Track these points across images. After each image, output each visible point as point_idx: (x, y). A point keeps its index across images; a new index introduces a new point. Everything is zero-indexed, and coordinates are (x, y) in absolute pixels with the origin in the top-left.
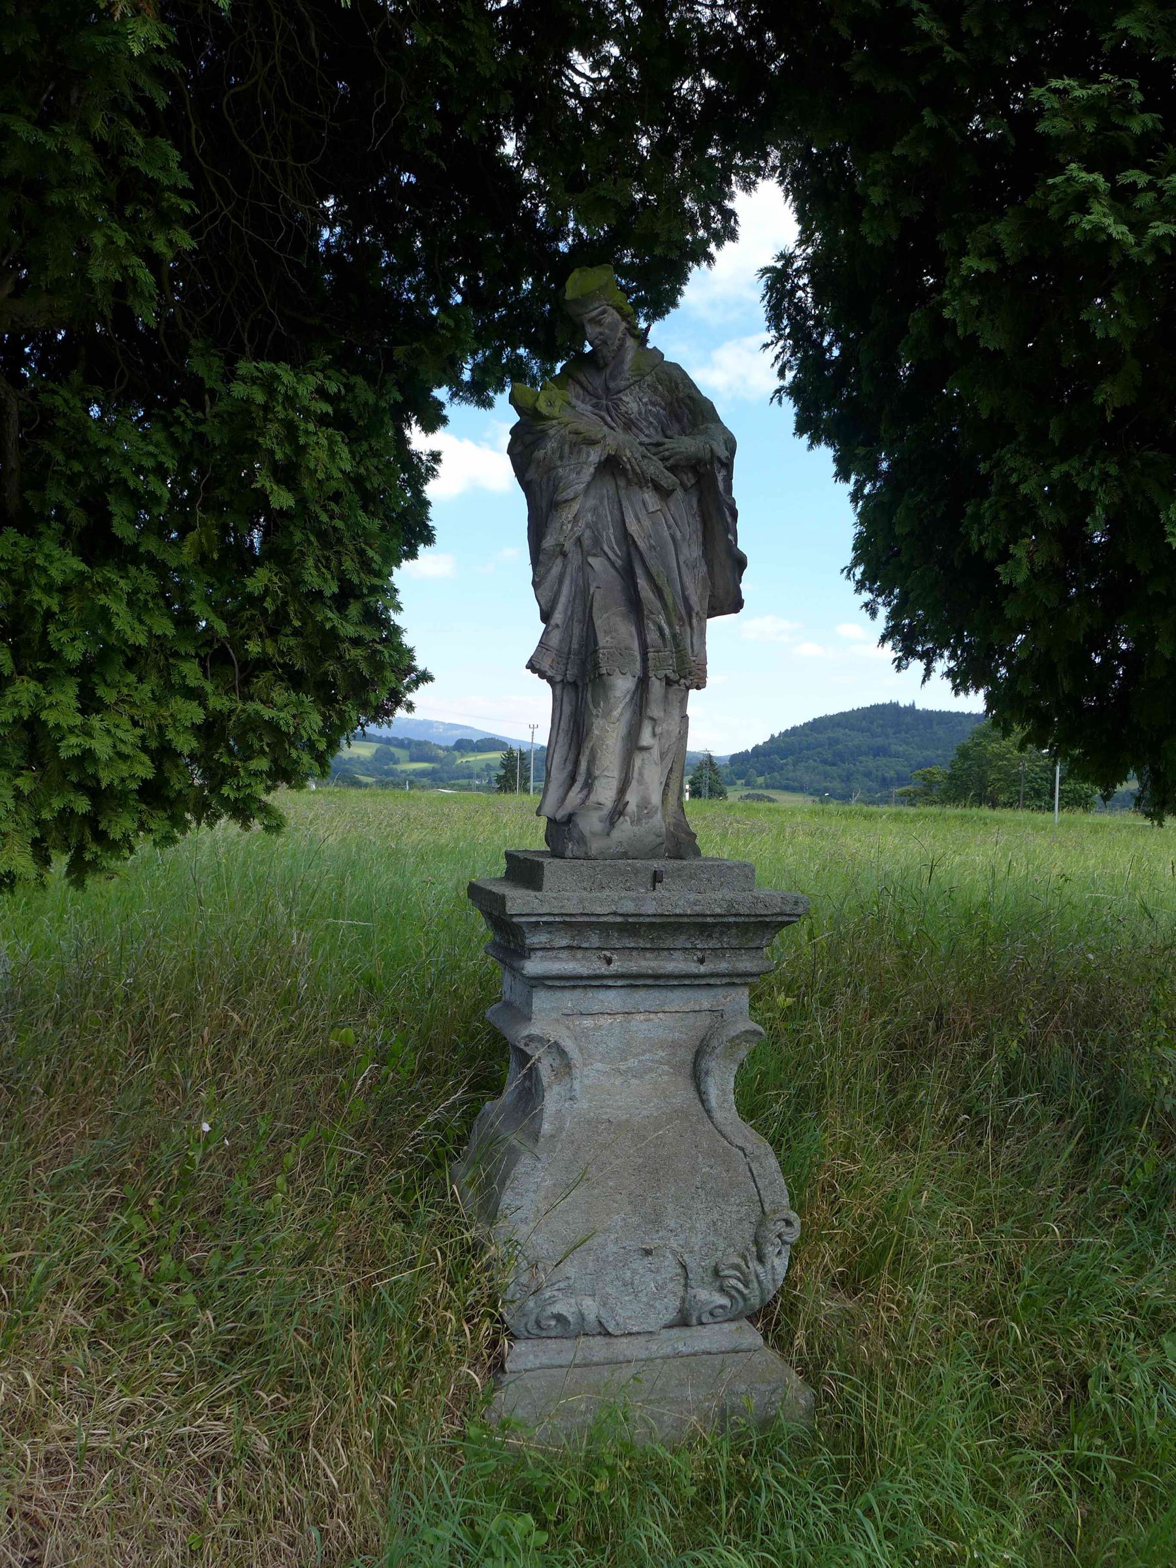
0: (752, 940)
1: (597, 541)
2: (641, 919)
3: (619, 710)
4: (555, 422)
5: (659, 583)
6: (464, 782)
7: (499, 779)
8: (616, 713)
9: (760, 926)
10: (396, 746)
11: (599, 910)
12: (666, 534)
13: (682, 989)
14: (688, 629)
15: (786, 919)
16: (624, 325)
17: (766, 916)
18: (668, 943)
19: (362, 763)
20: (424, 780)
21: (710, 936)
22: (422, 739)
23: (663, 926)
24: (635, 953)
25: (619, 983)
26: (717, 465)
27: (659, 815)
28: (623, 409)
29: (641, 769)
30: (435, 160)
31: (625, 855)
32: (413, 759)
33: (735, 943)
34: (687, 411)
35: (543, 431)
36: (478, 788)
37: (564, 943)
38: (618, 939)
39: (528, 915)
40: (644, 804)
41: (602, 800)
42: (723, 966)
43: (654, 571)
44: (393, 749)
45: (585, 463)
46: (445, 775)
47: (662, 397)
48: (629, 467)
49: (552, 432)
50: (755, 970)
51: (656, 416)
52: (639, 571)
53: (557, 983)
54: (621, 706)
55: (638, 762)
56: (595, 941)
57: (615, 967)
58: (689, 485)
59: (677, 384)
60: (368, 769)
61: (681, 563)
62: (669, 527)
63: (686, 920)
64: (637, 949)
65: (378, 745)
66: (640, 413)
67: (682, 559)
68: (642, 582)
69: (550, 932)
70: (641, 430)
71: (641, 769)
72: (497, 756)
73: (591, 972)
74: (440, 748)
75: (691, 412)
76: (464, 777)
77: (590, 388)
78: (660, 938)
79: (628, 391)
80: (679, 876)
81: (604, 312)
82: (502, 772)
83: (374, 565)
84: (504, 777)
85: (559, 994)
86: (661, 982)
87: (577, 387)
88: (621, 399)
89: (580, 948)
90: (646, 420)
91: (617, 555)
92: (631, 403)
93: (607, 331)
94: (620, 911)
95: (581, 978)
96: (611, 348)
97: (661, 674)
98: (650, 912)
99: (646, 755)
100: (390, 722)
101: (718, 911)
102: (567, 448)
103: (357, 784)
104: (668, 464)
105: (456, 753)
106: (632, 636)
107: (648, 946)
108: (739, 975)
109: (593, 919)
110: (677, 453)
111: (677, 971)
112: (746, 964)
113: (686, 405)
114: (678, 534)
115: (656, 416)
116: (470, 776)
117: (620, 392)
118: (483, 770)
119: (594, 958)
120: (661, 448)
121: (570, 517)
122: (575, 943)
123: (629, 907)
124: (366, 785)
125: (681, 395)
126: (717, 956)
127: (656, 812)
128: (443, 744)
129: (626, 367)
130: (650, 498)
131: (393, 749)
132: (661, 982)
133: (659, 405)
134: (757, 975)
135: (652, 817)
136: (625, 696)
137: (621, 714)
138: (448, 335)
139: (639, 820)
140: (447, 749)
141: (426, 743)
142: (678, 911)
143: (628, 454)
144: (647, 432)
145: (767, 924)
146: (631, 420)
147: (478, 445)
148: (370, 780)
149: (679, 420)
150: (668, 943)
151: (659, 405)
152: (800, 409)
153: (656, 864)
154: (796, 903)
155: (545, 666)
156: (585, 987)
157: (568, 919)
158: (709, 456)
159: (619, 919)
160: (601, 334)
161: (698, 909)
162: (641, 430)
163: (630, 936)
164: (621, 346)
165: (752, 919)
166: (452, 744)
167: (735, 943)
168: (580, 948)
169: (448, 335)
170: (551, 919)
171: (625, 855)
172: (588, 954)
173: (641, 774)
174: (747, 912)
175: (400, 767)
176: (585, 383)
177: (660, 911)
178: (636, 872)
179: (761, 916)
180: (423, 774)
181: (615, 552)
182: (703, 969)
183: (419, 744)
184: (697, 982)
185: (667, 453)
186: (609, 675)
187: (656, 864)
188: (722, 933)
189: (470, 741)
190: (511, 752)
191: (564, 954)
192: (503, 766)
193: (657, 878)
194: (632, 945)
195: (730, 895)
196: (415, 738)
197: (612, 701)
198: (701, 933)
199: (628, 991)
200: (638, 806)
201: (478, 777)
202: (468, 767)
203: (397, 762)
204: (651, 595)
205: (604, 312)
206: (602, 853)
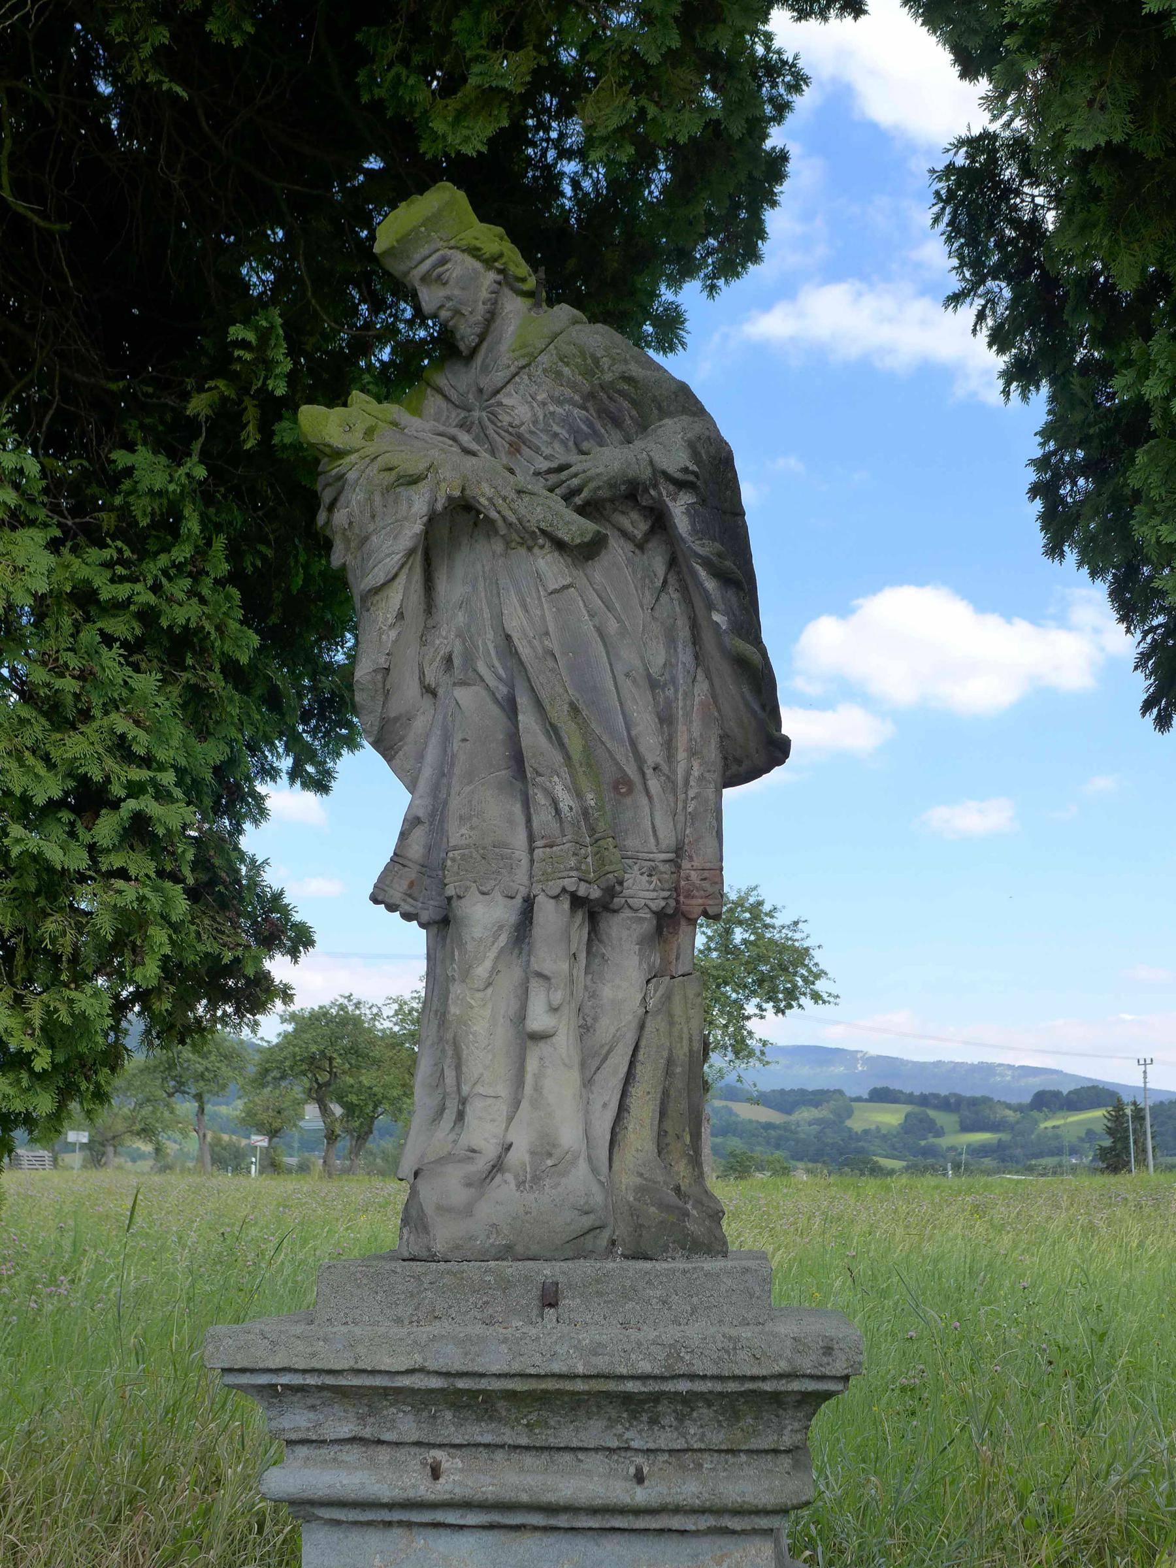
0: (755, 1433)
1: (469, 659)
2: (483, 1384)
3: (488, 964)
4: (353, 458)
5: (553, 715)
6: (1050, 1161)
7: (1103, 1154)
8: (482, 971)
9: (771, 1405)
10: (936, 1107)
11: (386, 1362)
12: (588, 627)
13: (617, 1538)
14: (644, 801)
15: (812, 1386)
16: (492, 276)
17: (764, 1378)
18: (567, 1436)
19: (885, 1138)
20: (986, 1160)
21: (654, 1421)
22: (978, 1095)
23: (543, 1399)
24: (500, 1455)
25: (472, 1519)
26: (665, 489)
27: (582, 1167)
28: (506, 419)
29: (538, 1077)
30: (165, 87)
31: (506, 1252)
32: (965, 1128)
33: (717, 1438)
34: (626, 404)
35: (340, 477)
36: (1073, 1170)
37: (346, 1430)
38: (458, 1426)
39: (243, 1371)
40: (545, 1147)
41: (477, 1143)
42: (690, 1490)
43: (544, 695)
44: (932, 1113)
45: (406, 518)
46: (1019, 1152)
47: (573, 386)
48: (494, 515)
49: (352, 476)
50: (767, 1500)
51: (565, 421)
52: (523, 701)
53: (451, 1518)
54: (492, 955)
55: (532, 1065)
56: (407, 1426)
57: (444, 1488)
58: (639, 535)
59: (596, 361)
60: (893, 1148)
61: (621, 677)
62: (592, 615)
63: (580, 1386)
64: (502, 1446)
65: (908, 1108)
66: (535, 422)
67: (619, 668)
68: (527, 719)
69: (313, 1408)
70: (537, 450)
71: (538, 1077)
72: (1097, 1116)
73: (397, 1494)
74: (1009, 1106)
75: (634, 403)
76: (1051, 1154)
77: (454, 396)
78: (547, 1425)
79: (510, 387)
80: (599, 1294)
81: (443, 261)
82: (1107, 1142)
83: (135, 748)
84: (1112, 1149)
85: (355, 1538)
86: (618, 1522)
87: (439, 398)
88: (500, 404)
89: (380, 1442)
90: (546, 431)
91: (500, 679)
92: (518, 407)
93: (457, 292)
94: (431, 1365)
95: (622, 1511)
96: (472, 319)
97: (555, 887)
98: (495, 1369)
99: (544, 1048)
100: (256, 1023)
101: (645, 1367)
102: (377, 498)
103: (876, 1171)
104: (578, 500)
105: (1035, 1113)
106: (511, 822)
107: (524, 1441)
108: (737, 1512)
109: (378, 1381)
110: (591, 479)
111: (583, 1499)
112: (747, 1484)
113: (621, 393)
114: (612, 626)
115: (565, 421)
116: (1058, 1152)
117: (498, 392)
118: (1081, 1140)
119: (414, 1464)
120: (564, 475)
121: (391, 617)
122: (367, 1433)
123: (451, 1358)
124: (891, 1172)
125: (608, 377)
126: (683, 1467)
127: (574, 1162)
128: (1014, 1101)
129: (503, 348)
130: (549, 566)
131: (932, 1113)
132: (562, 1521)
133: (571, 401)
134: (783, 1511)
135: (564, 1174)
136: (496, 938)
137: (495, 971)
138: (248, 356)
139: (536, 1179)
140: (1019, 1108)
141: (986, 1100)
142: (557, 1367)
143: (488, 490)
144: (547, 451)
145: (776, 1399)
146: (519, 436)
147: (1039, 626)
148: (898, 1164)
149: (617, 423)
150: (567, 1436)
151: (571, 401)
152: (1054, 392)
153: (548, 1270)
154: (828, 1350)
155: (396, 896)
156: (409, 1525)
157: (330, 1380)
158: (648, 472)
159: (436, 1383)
160: (449, 298)
161: (601, 1364)
162: (537, 450)
163: (479, 1420)
164: (491, 316)
165: (732, 1387)
166: (1027, 1099)
167: (717, 1438)
168: (380, 1442)
169: (248, 356)
170: (297, 1380)
171: (506, 1252)
172: (401, 1454)
173: (537, 1089)
174: (712, 1370)
175: (944, 1142)
176: (446, 389)
177: (516, 1367)
178: (506, 1285)
179: (753, 1378)
180: (982, 1151)
181: (495, 673)
182: (641, 1496)
183: (974, 1102)
184: (553, 1522)
185: (575, 482)
186: (459, 897)
187: (548, 1270)
188: (681, 1418)
189: (1057, 1094)
190: (1119, 1107)
191: (352, 1454)
192: (1110, 1132)
193: (550, 1299)
194: (487, 1439)
195: (671, 1333)
196: (968, 1094)
197: (470, 947)
198: (634, 1416)
199: (489, 1537)
200: (533, 1153)
201: (1073, 1151)
202: (1058, 1137)
203: (939, 1133)
204: (542, 741)
205: (443, 261)
206: (458, 1247)
